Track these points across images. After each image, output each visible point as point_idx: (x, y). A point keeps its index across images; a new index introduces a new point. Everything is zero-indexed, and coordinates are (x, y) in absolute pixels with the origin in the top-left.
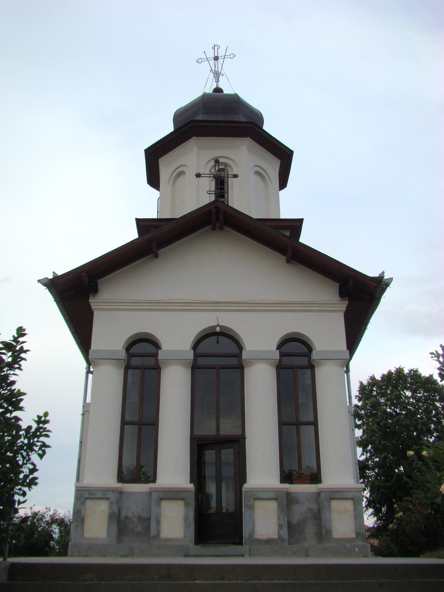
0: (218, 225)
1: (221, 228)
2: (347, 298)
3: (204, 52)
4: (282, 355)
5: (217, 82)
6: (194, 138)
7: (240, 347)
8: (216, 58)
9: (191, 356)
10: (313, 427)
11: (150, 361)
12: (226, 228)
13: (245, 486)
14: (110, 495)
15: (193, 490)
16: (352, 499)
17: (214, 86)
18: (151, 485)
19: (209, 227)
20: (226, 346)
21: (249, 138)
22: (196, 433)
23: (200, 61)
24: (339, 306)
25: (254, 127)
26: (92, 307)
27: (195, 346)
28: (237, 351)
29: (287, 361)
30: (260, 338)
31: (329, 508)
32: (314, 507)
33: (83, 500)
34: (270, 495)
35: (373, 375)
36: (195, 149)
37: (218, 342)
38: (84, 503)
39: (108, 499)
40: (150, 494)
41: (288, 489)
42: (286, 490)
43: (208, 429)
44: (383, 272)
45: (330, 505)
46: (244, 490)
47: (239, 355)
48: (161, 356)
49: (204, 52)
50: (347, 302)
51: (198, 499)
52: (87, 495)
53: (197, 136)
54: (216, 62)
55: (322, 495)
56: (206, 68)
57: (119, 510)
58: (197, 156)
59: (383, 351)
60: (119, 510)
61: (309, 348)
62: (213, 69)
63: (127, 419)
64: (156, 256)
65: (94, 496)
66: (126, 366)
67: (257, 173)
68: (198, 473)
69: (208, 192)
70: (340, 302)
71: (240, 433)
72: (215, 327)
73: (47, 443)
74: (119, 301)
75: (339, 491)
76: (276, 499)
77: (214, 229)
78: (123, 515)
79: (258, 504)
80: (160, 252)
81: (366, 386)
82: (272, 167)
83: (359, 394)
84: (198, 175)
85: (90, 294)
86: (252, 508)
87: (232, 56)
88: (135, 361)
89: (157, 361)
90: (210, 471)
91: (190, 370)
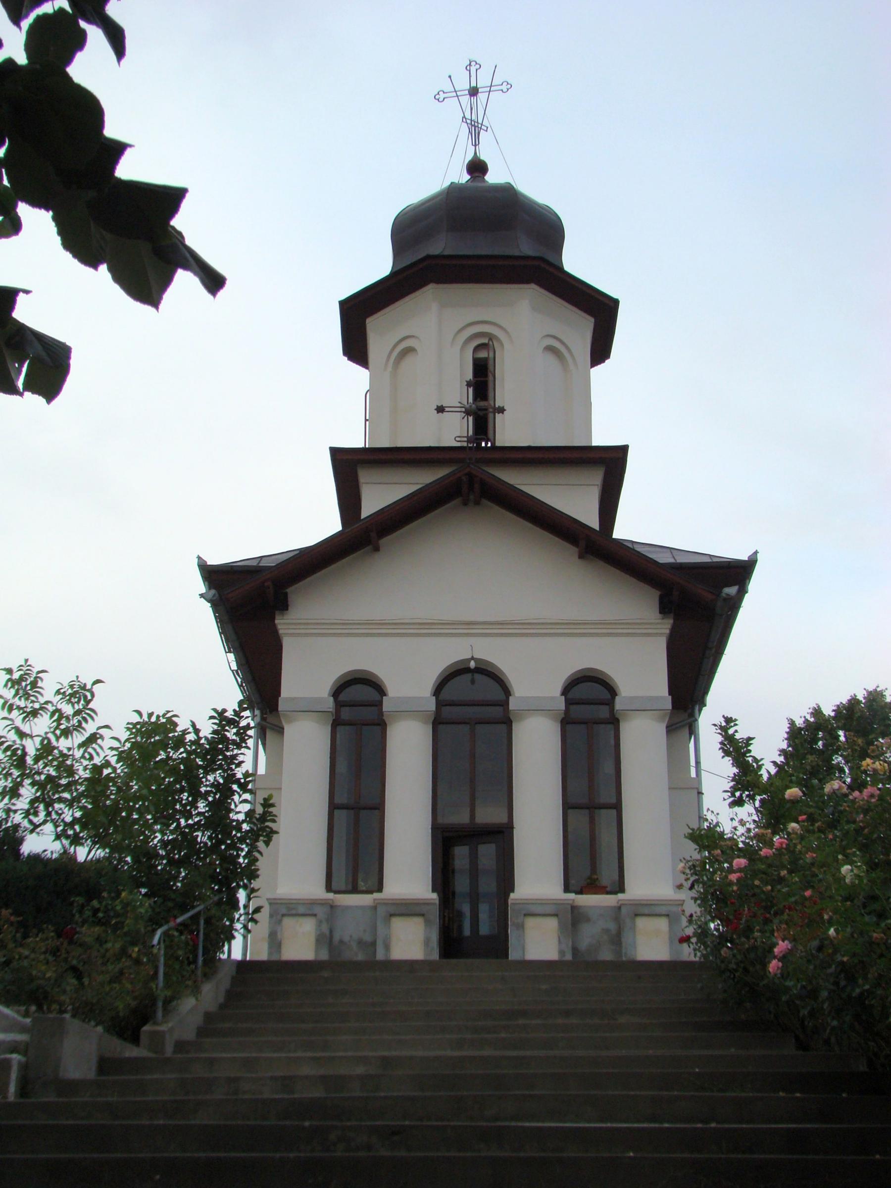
0: (472, 497)
1: (477, 503)
2: (672, 615)
3: (450, 77)
4: (569, 703)
5: (475, 145)
6: (431, 287)
7: (507, 691)
8: (474, 92)
9: (432, 706)
10: (614, 812)
11: (367, 713)
12: (485, 501)
13: (512, 896)
14: (317, 910)
15: (437, 902)
16: (668, 915)
17: (470, 157)
18: (376, 895)
19: (457, 501)
20: (485, 689)
21: (533, 286)
22: (440, 820)
23: (442, 96)
24: (659, 626)
25: (543, 265)
26: (281, 632)
27: (438, 690)
28: (502, 697)
29: (579, 711)
30: (535, 678)
31: (633, 928)
32: (612, 926)
33: (279, 917)
34: (549, 909)
35: (819, 706)
36: (435, 307)
37: (473, 682)
38: (280, 922)
39: (315, 915)
40: (374, 908)
41: (573, 900)
42: (571, 902)
43: (461, 818)
44: (756, 553)
45: (634, 923)
46: (510, 902)
47: (505, 704)
48: (387, 706)
49: (450, 77)
50: (671, 621)
51: (444, 916)
52: (284, 911)
53: (439, 281)
54: (474, 99)
55: (624, 910)
56: (453, 112)
57: (331, 931)
58: (438, 325)
59: (773, 679)
60: (331, 931)
61: (612, 691)
62: (468, 116)
63: (338, 800)
64: (377, 549)
65: (294, 912)
66: (334, 720)
67: (550, 349)
68: (443, 875)
69: (458, 439)
70: (660, 621)
71: (504, 819)
72: (469, 660)
73: (274, 829)
74: (323, 621)
75: (646, 905)
76: (556, 915)
77: (465, 503)
78: (337, 937)
79: (530, 922)
80: (383, 542)
81: (800, 729)
82: (579, 331)
83: (789, 746)
84: (440, 409)
85: (277, 612)
86: (521, 927)
87: (504, 87)
88: (346, 714)
89: (381, 713)
90: (461, 884)
91: (431, 726)
